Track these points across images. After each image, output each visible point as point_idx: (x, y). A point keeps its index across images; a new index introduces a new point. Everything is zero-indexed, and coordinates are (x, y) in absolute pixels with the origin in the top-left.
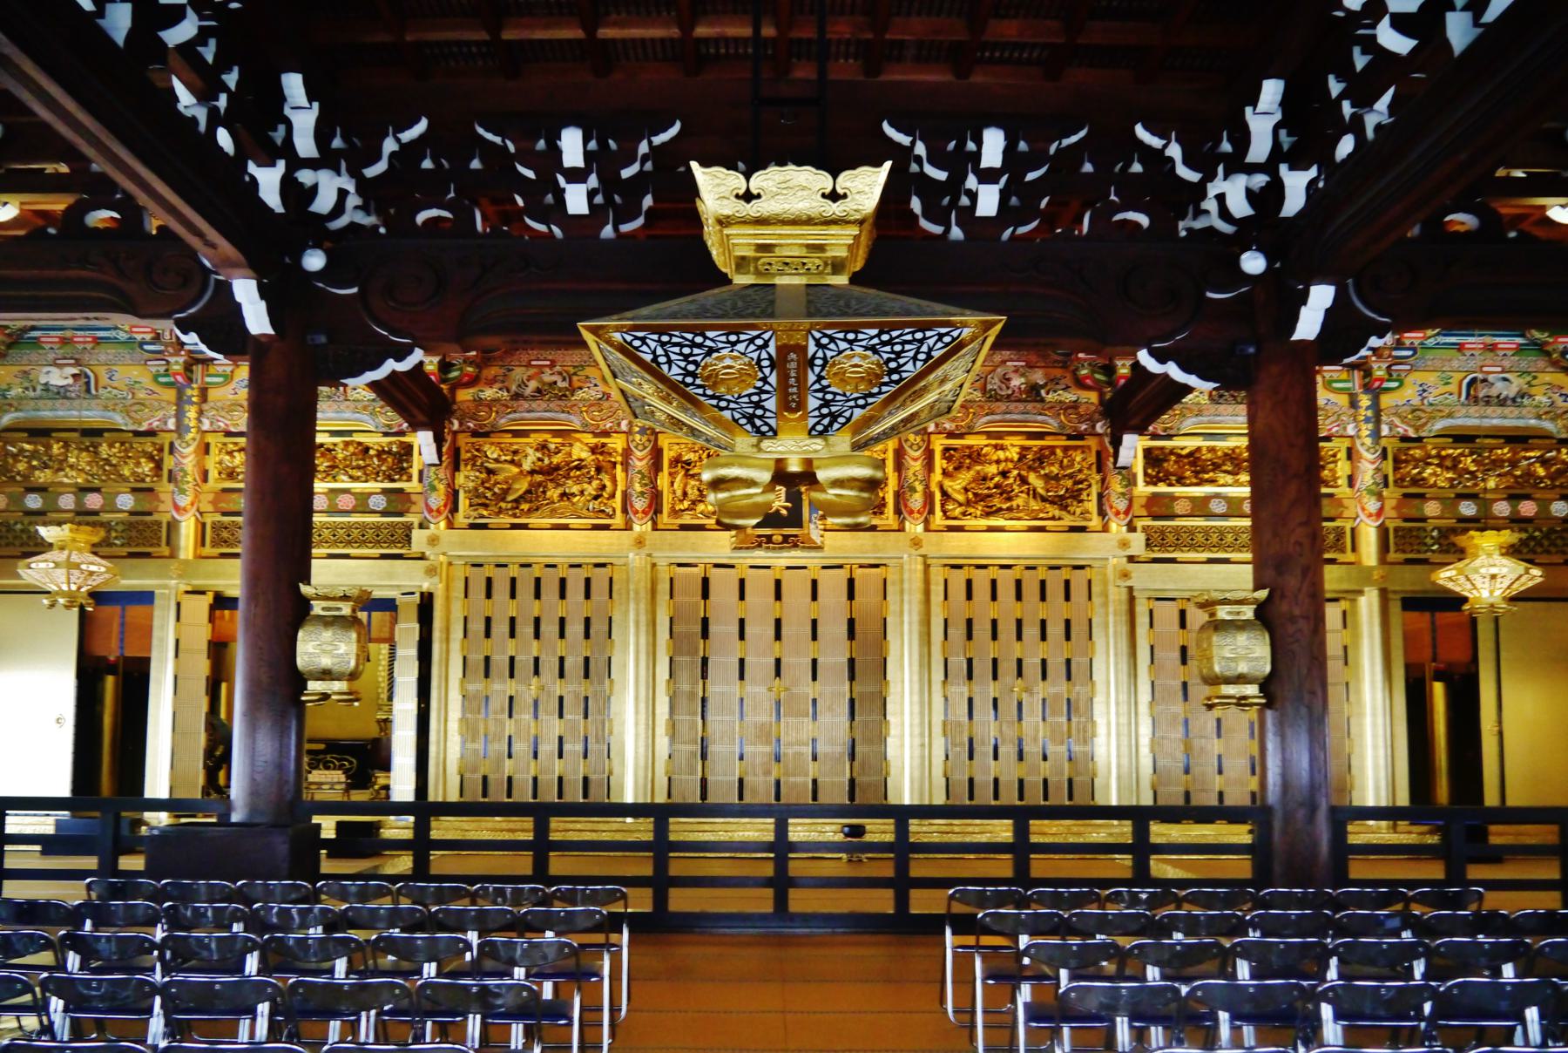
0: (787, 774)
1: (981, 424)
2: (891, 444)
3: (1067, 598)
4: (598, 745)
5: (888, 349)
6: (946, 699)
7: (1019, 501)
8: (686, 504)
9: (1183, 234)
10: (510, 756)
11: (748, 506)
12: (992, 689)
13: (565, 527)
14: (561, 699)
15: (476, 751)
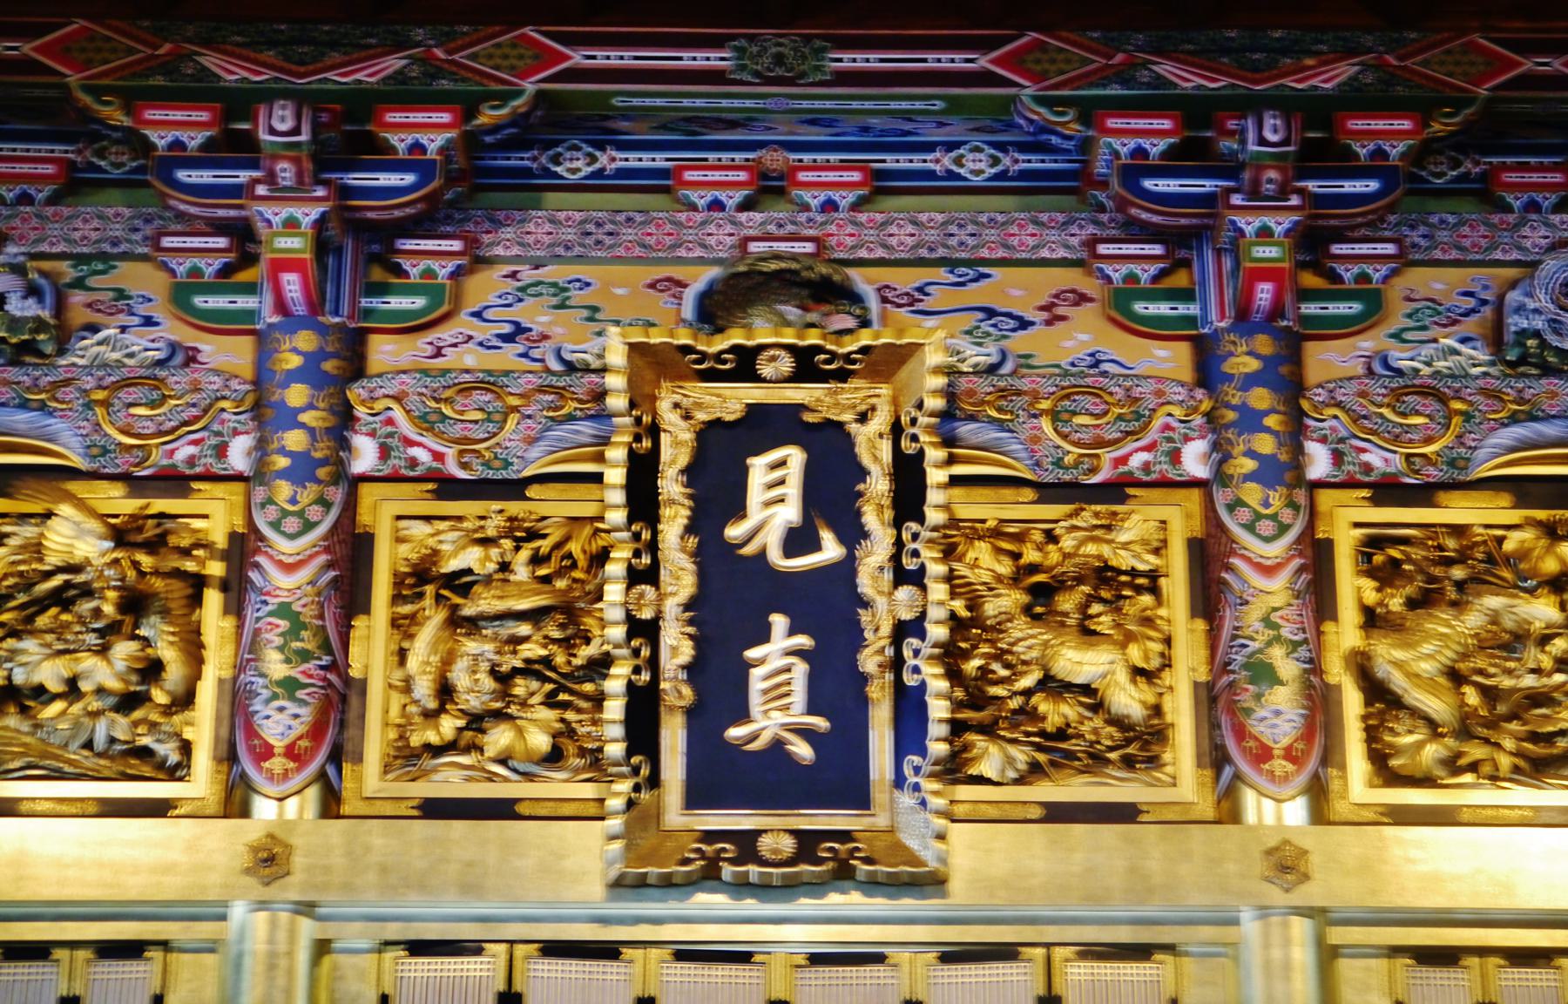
8: (449, 726)
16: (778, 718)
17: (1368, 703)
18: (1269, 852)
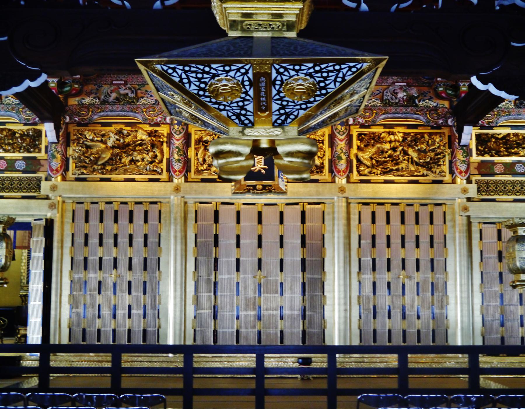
0: (265, 327)
1: (380, 120)
2: (327, 131)
3: (432, 223)
4: (152, 310)
5: (319, 75)
6: (360, 282)
7: (403, 165)
8: (205, 166)
9: (498, 8)
10: (99, 317)
11: (237, 167)
12: (387, 277)
13: (133, 180)
14: (130, 283)
15: (79, 314)
16: (259, 166)
17: (357, 162)
18: (339, 188)
